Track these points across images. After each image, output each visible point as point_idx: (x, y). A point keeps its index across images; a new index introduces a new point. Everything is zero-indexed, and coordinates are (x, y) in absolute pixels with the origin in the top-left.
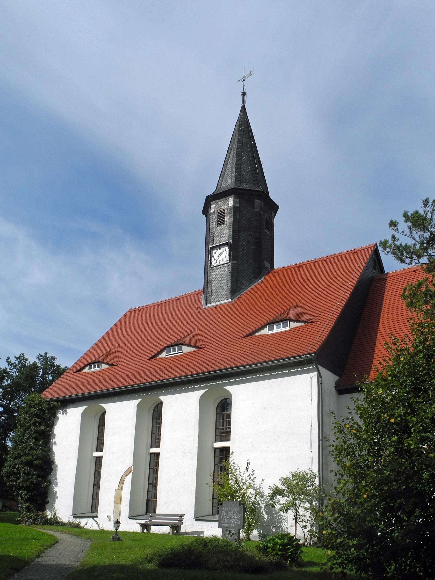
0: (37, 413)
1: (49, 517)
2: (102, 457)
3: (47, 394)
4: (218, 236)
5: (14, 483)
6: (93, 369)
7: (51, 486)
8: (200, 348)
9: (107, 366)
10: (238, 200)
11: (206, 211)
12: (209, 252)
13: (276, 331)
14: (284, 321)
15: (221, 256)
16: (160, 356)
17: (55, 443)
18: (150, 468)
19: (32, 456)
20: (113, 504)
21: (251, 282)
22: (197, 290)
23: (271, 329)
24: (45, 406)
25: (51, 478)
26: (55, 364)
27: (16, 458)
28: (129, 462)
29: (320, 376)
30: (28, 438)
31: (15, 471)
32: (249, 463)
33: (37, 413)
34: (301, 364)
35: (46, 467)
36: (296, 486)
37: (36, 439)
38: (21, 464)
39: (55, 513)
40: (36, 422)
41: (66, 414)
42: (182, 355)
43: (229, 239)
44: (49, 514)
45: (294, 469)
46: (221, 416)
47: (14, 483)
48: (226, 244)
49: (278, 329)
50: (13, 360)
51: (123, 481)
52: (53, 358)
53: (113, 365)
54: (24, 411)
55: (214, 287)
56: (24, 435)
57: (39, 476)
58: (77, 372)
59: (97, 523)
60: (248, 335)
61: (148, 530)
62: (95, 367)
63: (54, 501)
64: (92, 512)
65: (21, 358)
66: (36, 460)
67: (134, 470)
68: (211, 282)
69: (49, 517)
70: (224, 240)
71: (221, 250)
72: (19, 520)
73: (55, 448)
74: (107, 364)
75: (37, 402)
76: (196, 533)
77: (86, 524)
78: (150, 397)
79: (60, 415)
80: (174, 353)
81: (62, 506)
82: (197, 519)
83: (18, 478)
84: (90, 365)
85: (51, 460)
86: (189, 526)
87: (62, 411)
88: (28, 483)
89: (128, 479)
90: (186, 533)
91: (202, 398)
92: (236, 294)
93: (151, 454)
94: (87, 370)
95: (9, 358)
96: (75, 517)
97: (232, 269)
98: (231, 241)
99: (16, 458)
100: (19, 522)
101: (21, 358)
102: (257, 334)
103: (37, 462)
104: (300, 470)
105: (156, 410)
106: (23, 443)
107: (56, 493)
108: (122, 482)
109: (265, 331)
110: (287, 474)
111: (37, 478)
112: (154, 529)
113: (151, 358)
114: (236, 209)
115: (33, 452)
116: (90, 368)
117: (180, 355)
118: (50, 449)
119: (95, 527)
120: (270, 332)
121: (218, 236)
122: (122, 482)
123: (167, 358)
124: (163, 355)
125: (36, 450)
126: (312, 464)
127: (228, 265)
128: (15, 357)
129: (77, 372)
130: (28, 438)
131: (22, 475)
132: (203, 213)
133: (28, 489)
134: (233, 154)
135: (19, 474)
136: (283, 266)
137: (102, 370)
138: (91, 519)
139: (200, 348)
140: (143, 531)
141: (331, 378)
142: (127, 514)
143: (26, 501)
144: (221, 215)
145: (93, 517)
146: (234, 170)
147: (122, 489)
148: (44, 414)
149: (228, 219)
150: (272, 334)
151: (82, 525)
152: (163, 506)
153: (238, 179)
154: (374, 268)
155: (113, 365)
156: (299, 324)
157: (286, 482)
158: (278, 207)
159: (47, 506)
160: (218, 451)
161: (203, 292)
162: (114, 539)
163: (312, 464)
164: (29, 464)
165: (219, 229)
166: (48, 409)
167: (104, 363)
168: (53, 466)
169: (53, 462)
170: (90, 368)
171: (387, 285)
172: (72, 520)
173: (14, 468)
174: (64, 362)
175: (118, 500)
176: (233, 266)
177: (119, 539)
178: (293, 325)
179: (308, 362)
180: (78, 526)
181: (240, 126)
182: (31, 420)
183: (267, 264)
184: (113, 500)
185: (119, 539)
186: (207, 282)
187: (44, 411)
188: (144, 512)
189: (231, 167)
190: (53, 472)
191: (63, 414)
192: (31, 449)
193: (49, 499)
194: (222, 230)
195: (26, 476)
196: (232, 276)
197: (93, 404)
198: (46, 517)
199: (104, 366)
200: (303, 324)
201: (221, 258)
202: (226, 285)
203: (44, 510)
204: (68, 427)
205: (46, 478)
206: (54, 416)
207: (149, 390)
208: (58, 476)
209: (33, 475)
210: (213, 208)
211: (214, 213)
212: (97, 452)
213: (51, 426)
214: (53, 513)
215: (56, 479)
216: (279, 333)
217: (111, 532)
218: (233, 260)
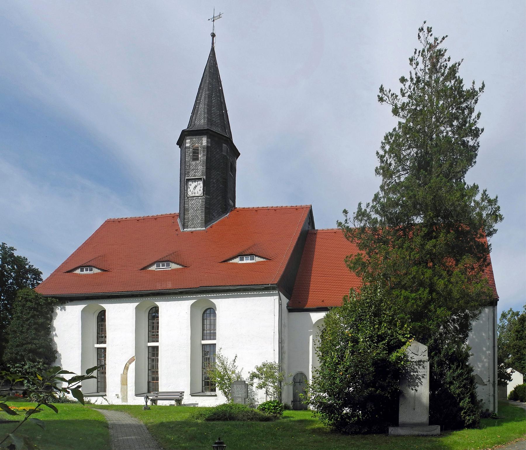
2: (215, 344)
4: (193, 170)
6: (85, 272)
8: (186, 267)
9: (99, 271)
10: (209, 140)
11: (181, 143)
12: (184, 183)
13: (245, 261)
14: (252, 255)
15: (196, 189)
16: (150, 269)
17: (56, 335)
18: (148, 358)
19: (35, 344)
20: (120, 386)
21: (220, 215)
22: (173, 212)
23: (242, 259)
24: (42, 301)
27: (17, 346)
28: (131, 353)
29: (280, 299)
30: (28, 329)
32: (236, 356)
34: (267, 289)
36: (265, 373)
40: (35, 315)
41: (65, 310)
42: (170, 270)
43: (202, 175)
45: (264, 361)
46: (205, 322)
48: (201, 179)
49: (247, 261)
51: (128, 368)
53: (106, 271)
55: (190, 214)
56: (22, 326)
58: (68, 272)
59: (106, 400)
60: (144, 268)
61: (156, 404)
66: (39, 348)
67: (136, 359)
68: (188, 210)
70: (199, 175)
71: (196, 183)
73: (56, 339)
74: (99, 269)
76: (192, 404)
77: (96, 401)
78: (149, 302)
79: (58, 310)
80: (163, 268)
82: (192, 395)
83: (24, 365)
84: (82, 267)
85: (54, 350)
86: (187, 400)
89: (132, 366)
90: (185, 405)
91: (192, 306)
92: (208, 223)
93: (149, 347)
94: (78, 271)
97: (206, 203)
98: (204, 177)
99: (17, 346)
102: (230, 262)
103: (40, 350)
104: (268, 361)
105: (151, 312)
106: (23, 332)
108: (126, 368)
109: (237, 260)
110: (260, 365)
111: (43, 365)
112: (160, 403)
113: (142, 269)
114: (208, 149)
115: (36, 341)
116: (82, 271)
117: (168, 270)
118: (52, 340)
119: (105, 403)
120: (240, 262)
121: (193, 170)
122: (126, 368)
123: (157, 271)
124: (154, 268)
125: (38, 340)
126: (275, 358)
127: (202, 198)
129: (68, 272)
130: (28, 329)
132: (177, 144)
134: (205, 95)
136: (243, 207)
137: (94, 274)
139: (186, 267)
140: (152, 405)
141: (285, 300)
142: (134, 393)
144: (196, 152)
145: (102, 396)
146: (206, 111)
147: (127, 374)
148: (42, 309)
149: (201, 156)
150: (242, 264)
152: (164, 386)
153: (210, 121)
154: (309, 224)
155: (106, 271)
156: (262, 260)
157: (259, 369)
158: (239, 154)
160: (150, 348)
161: (179, 215)
163: (275, 358)
165: (194, 163)
166: (45, 304)
167: (96, 268)
168: (56, 355)
169: (57, 352)
170: (82, 271)
171: (317, 240)
175: (124, 382)
176: (206, 199)
178: (258, 259)
179: (274, 289)
181: (210, 68)
182: (29, 313)
183: (231, 202)
184: (119, 382)
186: (184, 209)
188: (146, 391)
189: (202, 107)
190: (57, 360)
191: (61, 310)
192: (34, 339)
194: (196, 165)
196: (206, 208)
199: (96, 271)
200: (265, 260)
201: (196, 191)
202: (200, 216)
206: (52, 311)
207: (147, 295)
209: (39, 362)
210: (188, 143)
211: (189, 148)
216: (247, 264)
218: (206, 194)
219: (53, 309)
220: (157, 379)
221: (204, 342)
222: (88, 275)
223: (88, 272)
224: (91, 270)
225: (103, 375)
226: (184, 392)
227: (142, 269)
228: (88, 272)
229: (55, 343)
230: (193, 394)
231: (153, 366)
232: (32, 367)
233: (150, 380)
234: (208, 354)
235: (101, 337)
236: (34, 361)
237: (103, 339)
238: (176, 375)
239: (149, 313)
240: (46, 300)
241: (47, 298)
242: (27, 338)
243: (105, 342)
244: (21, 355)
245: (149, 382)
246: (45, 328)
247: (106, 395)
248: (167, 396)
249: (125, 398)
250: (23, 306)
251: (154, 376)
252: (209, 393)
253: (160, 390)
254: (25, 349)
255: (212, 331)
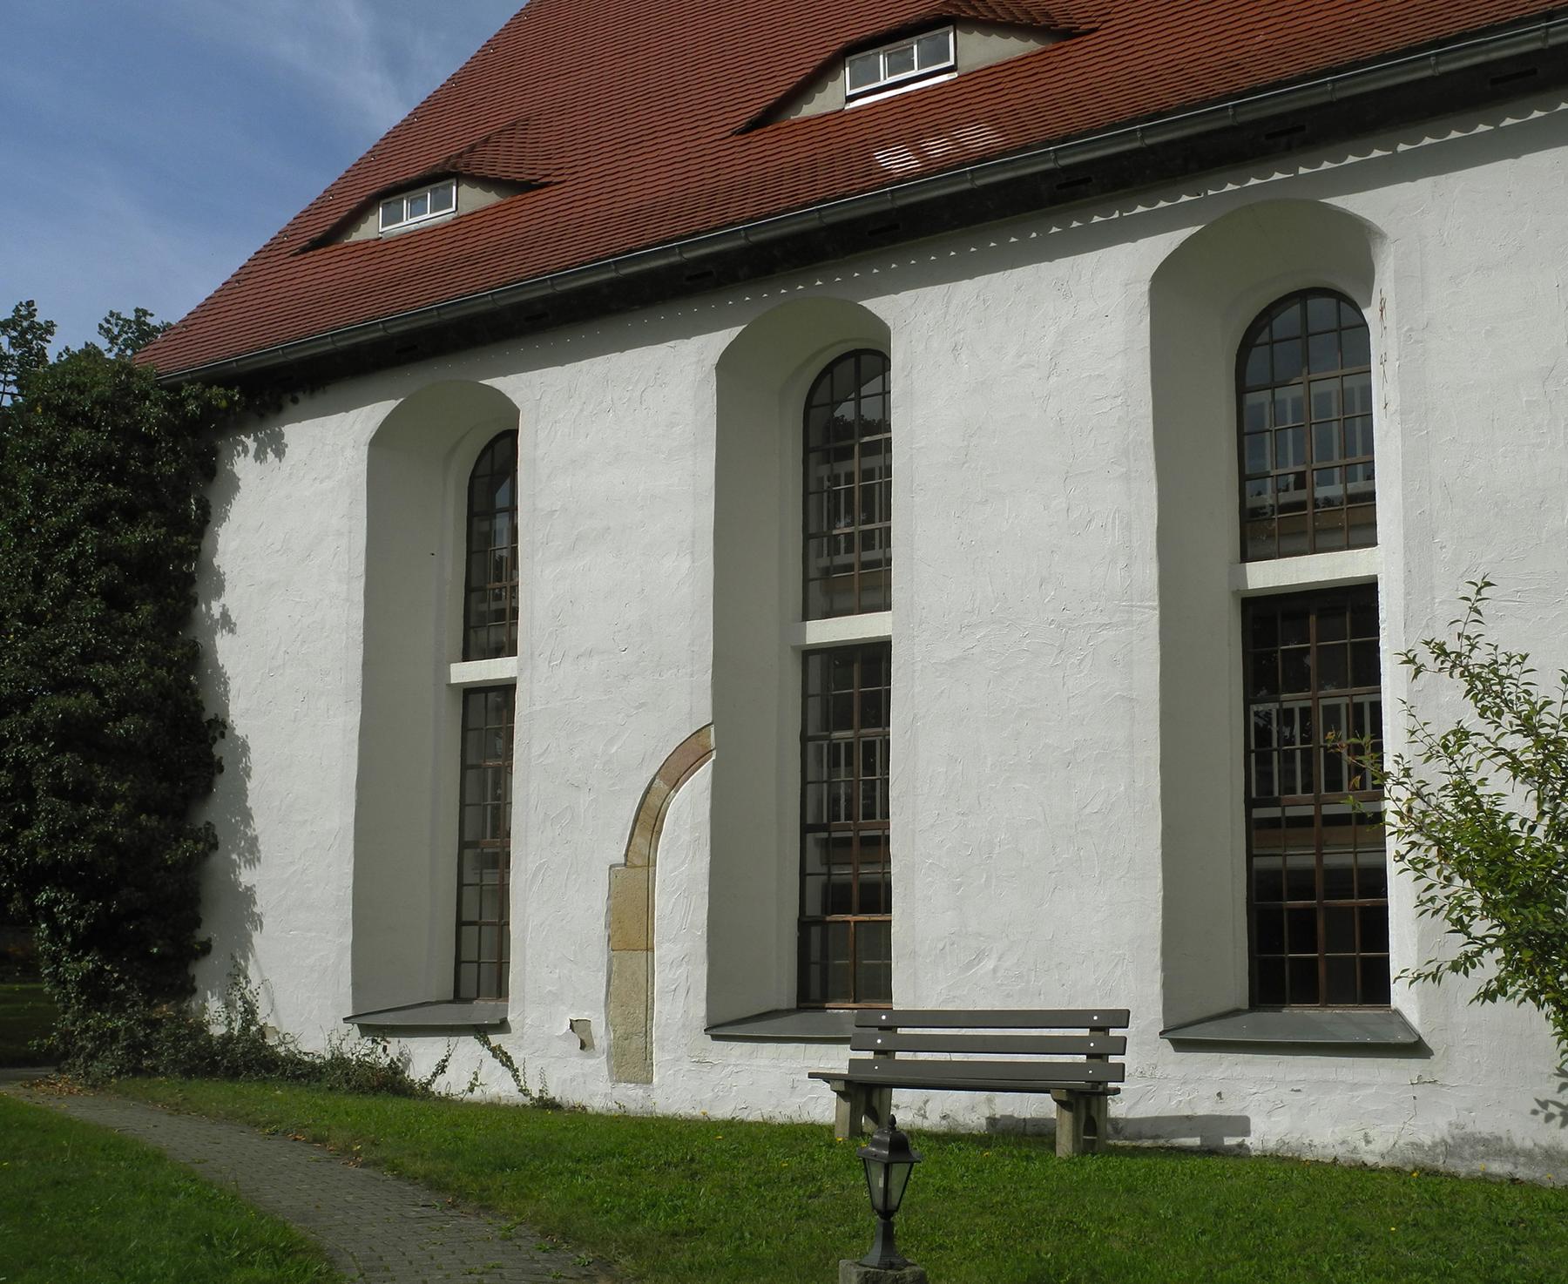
17: (226, 622)
19: (98, 692)
28: (687, 702)
51: (659, 818)
59: (507, 1061)
66: (118, 717)
73: (228, 652)
76: (1189, 1123)
77: (442, 1068)
78: (805, 307)
79: (245, 466)
85: (208, 715)
86: (1158, 1086)
89: (691, 804)
105: (822, 396)
108: (649, 820)
113: (746, 131)
115: (101, 672)
119: (499, 1086)
122: (649, 820)
125: (117, 661)
129: (316, 244)
130: (65, 598)
142: (699, 1011)
145: (481, 1031)
147: (650, 863)
148: (148, 462)
152: (940, 955)
160: (815, 662)
168: (219, 750)
169: (220, 726)
175: (631, 926)
190: (221, 784)
191: (260, 456)
207: (795, 263)
209: (108, 800)
220: (878, 897)
221: (1267, 575)
225: (490, 878)
226: (1122, 1018)
227: (746, 131)
229: (218, 669)
230: (1185, 1036)
231: (834, 801)
232: (71, 833)
233: (814, 909)
234: (1298, 675)
235: (489, 617)
236: (79, 794)
237: (496, 635)
238: (1044, 869)
239: (809, 406)
240: (175, 406)
241: (175, 388)
242: (56, 652)
243: (507, 648)
244: (19, 763)
245: (804, 924)
246: (164, 582)
247: (502, 1026)
248: (982, 1046)
249: (632, 1059)
250: (50, 454)
251: (843, 873)
253: (904, 997)
254: (40, 725)
255: (1360, 457)
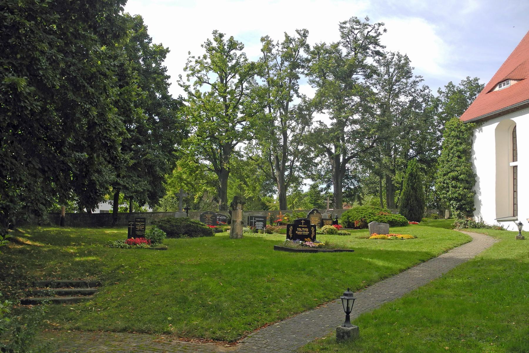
0: (457, 135)
1: (477, 222)
3: (466, 116)
5: (445, 196)
7: (476, 195)
9: (516, 82)
17: (476, 158)
25: (475, 188)
26: (480, 84)
27: (444, 175)
30: (452, 157)
31: (445, 185)
33: (457, 135)
35: (470, 180)
37: (459, 157)
38: (449, 179)
39: (482, 219)
44: (477, 219)
47: (445, 196)
50: (444, 90)
52: (476, 80)
53: (522, 80)
54: (447, 134)
56: (449, 155)
57: (465, 188)
58: (489, 92)
62: (504, 85)
63: (480, 208)
64: (514, 216)
65: (450, 86)
69: (477, 222)
72: (454, 226)
73: (476, 163)
74: (515, 80)
75: (456, 125)
81: (487, 212)
83: (448, 191)
84: (499, 84)
87: (478, 130)
88: (456, 195)
94: (497, 89)
95: (440, 88)
96: (498, 221)
100: (454, 227)
101: (450, 86)
103: (462, 176)
106: (449, 161)
107: (480, 201)
118: (472, 164)
128: (445, 86)
129: (489, 92)
130: (452, 157)
131: (451, 189)
133: (457, 200)
135: (449, 187)
137: (511, 87)
138: (512, 222)
143: (457, 209)
148: (463, 135)
151: (505, 227)
155: (522, 80)
159: (474, 213)
162: (518, 238)
164: (455, 178)
167: (512, 80)
169: (476, 175)
172: (496, 223)
173: (444, 183)
174: (484, 81)
177: (523, 238)
180: (501, 229)
185: (523, 238)
187: (463, 132)
190: (476, 183)
191: (479, 132)
193: (475, 207)
195: (454, 189)
197: (504, 119)
198: (475, 221)
199: (512, 83)
203: (472, 216)
204: (485, 143)
205: (471, 189)
206: (472, 134)
208: (480, 186)
209: (459, 188)
212: (513, 161)
213: (471, 144)
214: (480, 218)
215: (480, 189)
217: (515, 233)
219: (473, 132)
222: (505, 89)
223: (506, 86)
224: (508, 84)
228: (506, 86)
236: (455, 187)
252: (365, 229)
